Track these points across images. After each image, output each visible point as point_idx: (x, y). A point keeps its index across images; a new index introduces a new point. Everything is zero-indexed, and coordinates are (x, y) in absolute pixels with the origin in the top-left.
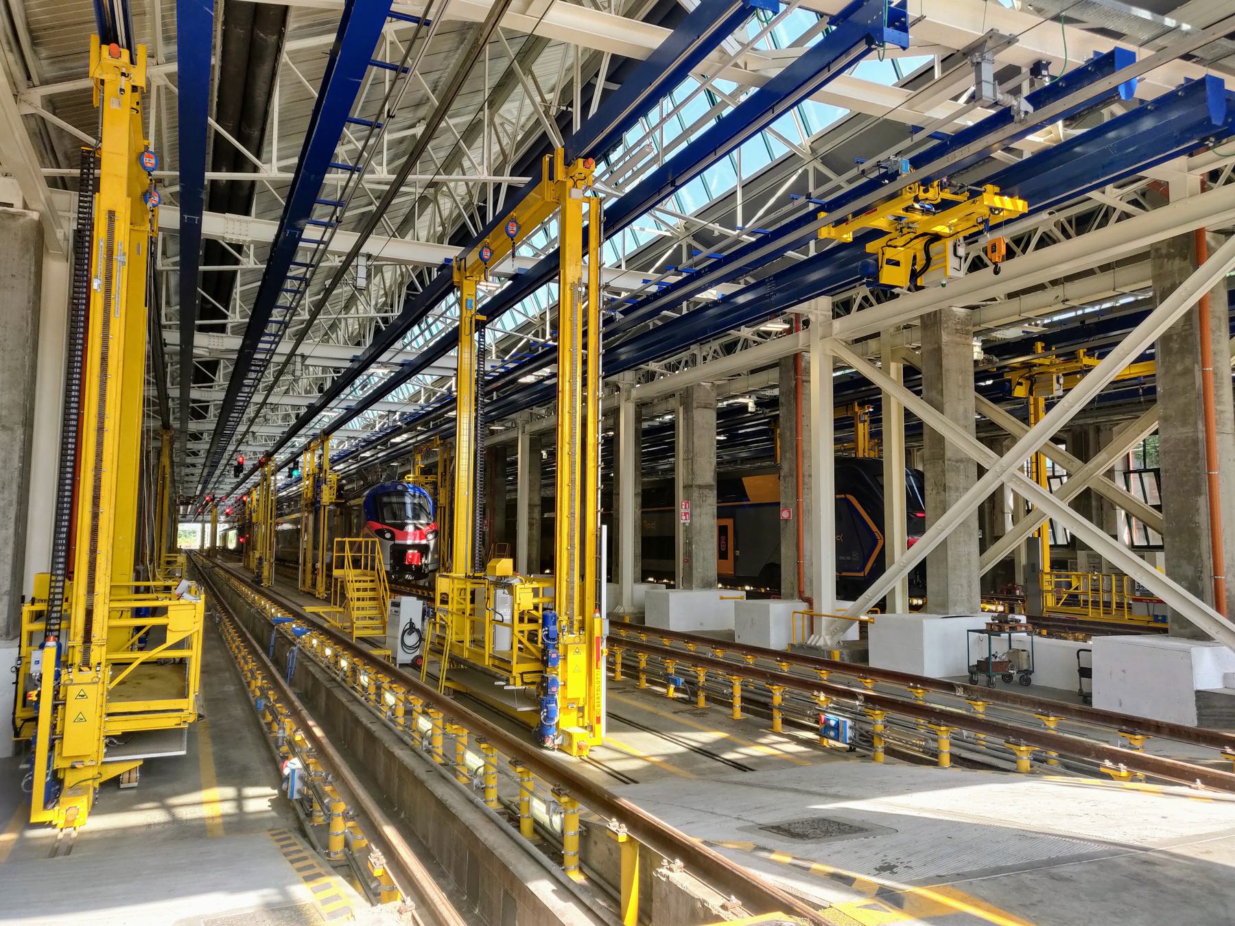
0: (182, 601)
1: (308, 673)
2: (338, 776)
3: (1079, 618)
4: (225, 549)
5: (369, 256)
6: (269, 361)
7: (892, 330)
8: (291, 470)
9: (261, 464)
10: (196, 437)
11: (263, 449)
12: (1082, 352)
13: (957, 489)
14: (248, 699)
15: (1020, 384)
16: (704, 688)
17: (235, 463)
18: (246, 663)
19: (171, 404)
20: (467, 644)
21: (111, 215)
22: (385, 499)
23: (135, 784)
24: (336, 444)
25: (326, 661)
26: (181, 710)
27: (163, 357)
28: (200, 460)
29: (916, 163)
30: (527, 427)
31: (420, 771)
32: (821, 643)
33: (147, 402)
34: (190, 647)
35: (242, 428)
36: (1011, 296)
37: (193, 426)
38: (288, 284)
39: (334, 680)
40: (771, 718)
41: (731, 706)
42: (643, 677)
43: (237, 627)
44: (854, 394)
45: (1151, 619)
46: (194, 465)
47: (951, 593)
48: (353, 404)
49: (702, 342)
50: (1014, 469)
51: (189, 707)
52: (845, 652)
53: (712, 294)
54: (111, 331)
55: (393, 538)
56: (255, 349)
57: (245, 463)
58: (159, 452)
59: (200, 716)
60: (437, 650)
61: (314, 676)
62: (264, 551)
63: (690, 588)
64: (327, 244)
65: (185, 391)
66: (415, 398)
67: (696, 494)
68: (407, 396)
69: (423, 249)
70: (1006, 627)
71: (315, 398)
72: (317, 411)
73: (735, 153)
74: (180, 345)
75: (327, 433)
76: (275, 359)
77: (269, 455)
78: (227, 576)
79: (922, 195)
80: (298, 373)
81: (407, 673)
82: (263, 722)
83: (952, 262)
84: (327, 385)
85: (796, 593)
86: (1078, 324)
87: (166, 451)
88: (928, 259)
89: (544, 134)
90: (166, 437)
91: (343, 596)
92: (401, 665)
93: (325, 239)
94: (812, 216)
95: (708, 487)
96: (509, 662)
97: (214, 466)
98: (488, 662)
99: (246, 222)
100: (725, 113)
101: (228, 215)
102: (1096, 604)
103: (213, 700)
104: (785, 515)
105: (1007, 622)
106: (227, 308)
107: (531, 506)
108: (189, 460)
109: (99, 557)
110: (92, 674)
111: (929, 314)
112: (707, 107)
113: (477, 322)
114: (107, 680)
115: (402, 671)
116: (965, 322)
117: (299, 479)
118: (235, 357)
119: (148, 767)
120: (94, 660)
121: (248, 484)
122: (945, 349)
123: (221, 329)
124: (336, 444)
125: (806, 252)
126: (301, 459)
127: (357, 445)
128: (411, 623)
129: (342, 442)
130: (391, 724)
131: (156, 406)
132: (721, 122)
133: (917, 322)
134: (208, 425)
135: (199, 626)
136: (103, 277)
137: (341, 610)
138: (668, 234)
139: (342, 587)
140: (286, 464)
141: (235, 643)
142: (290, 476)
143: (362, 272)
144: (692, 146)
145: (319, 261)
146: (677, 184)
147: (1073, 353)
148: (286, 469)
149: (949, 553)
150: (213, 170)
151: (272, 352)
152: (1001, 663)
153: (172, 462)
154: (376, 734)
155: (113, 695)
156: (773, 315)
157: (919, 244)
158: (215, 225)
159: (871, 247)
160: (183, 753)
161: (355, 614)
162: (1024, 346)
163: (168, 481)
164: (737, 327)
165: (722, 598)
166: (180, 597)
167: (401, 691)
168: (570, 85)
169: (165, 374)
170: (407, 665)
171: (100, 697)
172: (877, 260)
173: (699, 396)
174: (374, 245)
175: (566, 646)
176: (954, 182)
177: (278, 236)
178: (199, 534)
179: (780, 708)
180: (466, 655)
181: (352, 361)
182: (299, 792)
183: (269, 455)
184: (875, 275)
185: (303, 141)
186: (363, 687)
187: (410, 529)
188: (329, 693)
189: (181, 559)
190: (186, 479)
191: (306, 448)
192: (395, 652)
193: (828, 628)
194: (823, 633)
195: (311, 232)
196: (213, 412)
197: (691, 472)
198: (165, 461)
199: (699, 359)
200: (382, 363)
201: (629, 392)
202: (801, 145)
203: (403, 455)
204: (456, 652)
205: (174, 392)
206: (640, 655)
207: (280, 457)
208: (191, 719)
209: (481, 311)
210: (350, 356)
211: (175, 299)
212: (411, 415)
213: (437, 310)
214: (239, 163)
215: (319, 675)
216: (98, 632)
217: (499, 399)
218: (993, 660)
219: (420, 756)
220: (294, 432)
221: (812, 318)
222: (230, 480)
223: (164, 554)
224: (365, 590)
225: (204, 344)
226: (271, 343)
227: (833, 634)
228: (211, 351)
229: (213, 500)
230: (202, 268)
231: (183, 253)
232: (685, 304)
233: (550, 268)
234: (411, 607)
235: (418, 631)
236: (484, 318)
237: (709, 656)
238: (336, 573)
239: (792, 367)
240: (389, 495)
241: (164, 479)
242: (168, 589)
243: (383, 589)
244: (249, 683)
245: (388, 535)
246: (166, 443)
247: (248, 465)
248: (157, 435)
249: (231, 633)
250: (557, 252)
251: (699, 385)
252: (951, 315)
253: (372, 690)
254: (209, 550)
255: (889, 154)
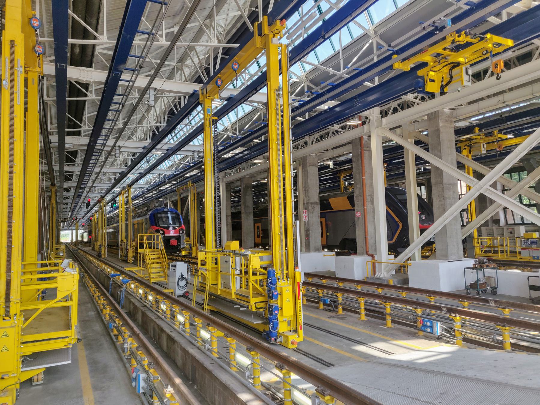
0: (65, 273)
1: (130, 302)
2: (157, 363)
3: (494, 258)
4: (82, 242)
5: (155, 89)
6: (103, 150)
7: (408, 123)
8: (112, 204)
9: (99, 202)
10: (67, 190)
11: (99, 195)
12: (496, 132)
13: (450, 198)
14: (102, 320)
15: (465, 149)
16: (341, 304)
17: (86, 202)
18: (100, 299)
19: (55, 174)
20: (220, 286)
21: (12, 43)
22: (159, 215)
23: (42, 382)
24: (134, 191)
25: (140, 296)
26: (67, 337)
27: (50, 149)
28: (69, 201)
29: (455, 21)
30: (225, 179)
31: (207, 364)
32: (382, 276)
33: (41, 173)
34: (71, 299)
35: (89, 185)
36: (469, 103)
37: (66, 184)
38: (90, 165)
39: (145, 306)
40: (385, 319)
41: (359, 313)
42: (340, 308)
43: (91, 278)
44: (393, 154)
45: (532, 258)
46: (67, 204)
47: (449, 250)
48: (142, 171)
49: (310, 135)
50: (487, 186)
51: (72, 334)
52: (396, 280)
53: (325, 107)
54: (15, 113)
55: (164, 233)
56: (95, 142)
57: (91, 202)
58: (50, 197)
59: (78, 339)
60: (202, 289)
61: (134, 304)
62: (102, 243)
63: (309, 251)
64: (134, 82)
65: (61, 166)
66: (171, 167)
67: (310, 207)
68: (166, 168)
69: (181, 86)
70: (485, 266)
71: (147, 143)
72: (129, 170)
73: (236, 109)
74: (58, 143)
75: (130, 185)
76: (106, 149)
77: (103, 197)
78: (85, 254)
79: (457, 39)
80: (117, 155)
81: (182, 300)
82: (112, 334)
83: (465, 78)
84: (129, 163)
85: (365, 252)
86: (499, 117)
87: (53, 196)
88: (451, 77)
89: (244, 23)
90: (53, 190)
91: (144, 262)
92: (178, 296)
93: (133, 79)
94: (389, 58)
95: (316, 203)
96: (248, 297)
97: (77, 204)
98: (234, 297)
99: (91, 71)
100: (327, 18)
101: (80, 68)
102: (502, 252)
103: (83, 321)
104: (358, 214)
105: (484, 263)
106: (81, 123)
107: (227, 216)
108: (64, 201)
109: (13, 250)
110: (12, 321)
111: (432, 113)
112: (257, 68)
113: (213, 121)
114: (21, 323)
115: (178, 299)
116: (450, 116)
117: (117, 208)
118: (86, 148)
119: (48, 372)
120: (12, 311)
121: (92, 212)
122: (441, 130)
123: (78, 134)
124: (134, 191)
125: (304, 118)
126: (117, 199)
127: (143, 191)
128: (182, 275)
129: (136, 190)
130: (183, 333)
131: (47, 175)
132: (325, 23)
133: (426, 118)
134: (73, 184)
135: (76, 288)
136: (8, 80)
137: (143, 269)
138: (298, 80)
139: (143, 258)
140: (110, 201)
141: (93, 289)
142: (112, 207)
143: (152, 98)
144: (309, 37)
145: (125, 101)
146: (326, 37)
147: (491, 133)
148: (110, 204)
149: (447, 230)
150: (72, 38)
151: (104, 145)
152: (483, 284)
153: (57, 203)
154: (176, 338)
155: (24, 331)
156: (352, 117)
157: (446, 70)
158: (75, 73)
159: (420, 73)
160: (69, 362)
161: (151, 270)
162: (469, 130)
163: (55, 211)
164: (406, 94)
165: (324, 256)
166: (64, 270)
167: (188, 314)
168: (208, 58)
169: (51, 159)
170: (181, 296)
171: (17, 335)
172: (424, 80)
173: (310, 161)
174: (157, 84)
175: (281, 288)
176: (472, 32)
177: (108, 78)
178: (70, 235)
179: (390, 315)
180: (219, 293)
181: (143, 148)
182: (143, 388)
183: (103, 197)
184: (423, 87)
185: (117, 34)
186: (163, 310)
187: (171, 228)
188: (144, 314)
189: (63, 247)
190: (64, 210)
191: (120, 193)
192: (175, 290)
193: (385, 269)
194: (383, 271)
195: (125, 76)
196: (75, 179)
197: (307, 197)
198: (53, 201)
199: (309, 143)
200: (158, 149)
201: (223, 180)
202: (369, 29)
203: (164, 194)
204: (213, 291)
205: (56, 168)
206: (322, 291)
207: (108, 198)
208: (73, 342)
209: (215, 115)
210: (142, 146)
211: (55, 121)
212: (170, 175)
213: (179, 127)
214: (86, 35)
215: (137, 304)
216: (15, 296)
217: (180, 182)
218: (479, 282)
219: (205, 353)
220: (114, 186)
221: (371, 118)
222: (84, 210)
223: (54, 245)
224: (154, 259)
225: (70, 142)
226: (104, 140)
227: (388, 272)
228: (74, 145)
229: (76, 219)
230: (68, 99)
231: (58, 123)
232: (307, 114)
233: (262, 81)
234: (182, 267)
235: (185, 279)
236: (216, 118)
237: (335, 286)
238: (140, 251)
239: (360, 145)
240: (160, 213)
241: (53, 210)
242: (56, 265)
243: (164, 257)
244: (102, 310)
245: (161, 232)
246: (53, 193)
247: (92, 202)
248: (48, 190)
249: (90, 283)
250: (203, 123)
251: (310, 155)
252: (444, 112)
253: (169, 312)
254: (75, 242)
255: (441, 15)
